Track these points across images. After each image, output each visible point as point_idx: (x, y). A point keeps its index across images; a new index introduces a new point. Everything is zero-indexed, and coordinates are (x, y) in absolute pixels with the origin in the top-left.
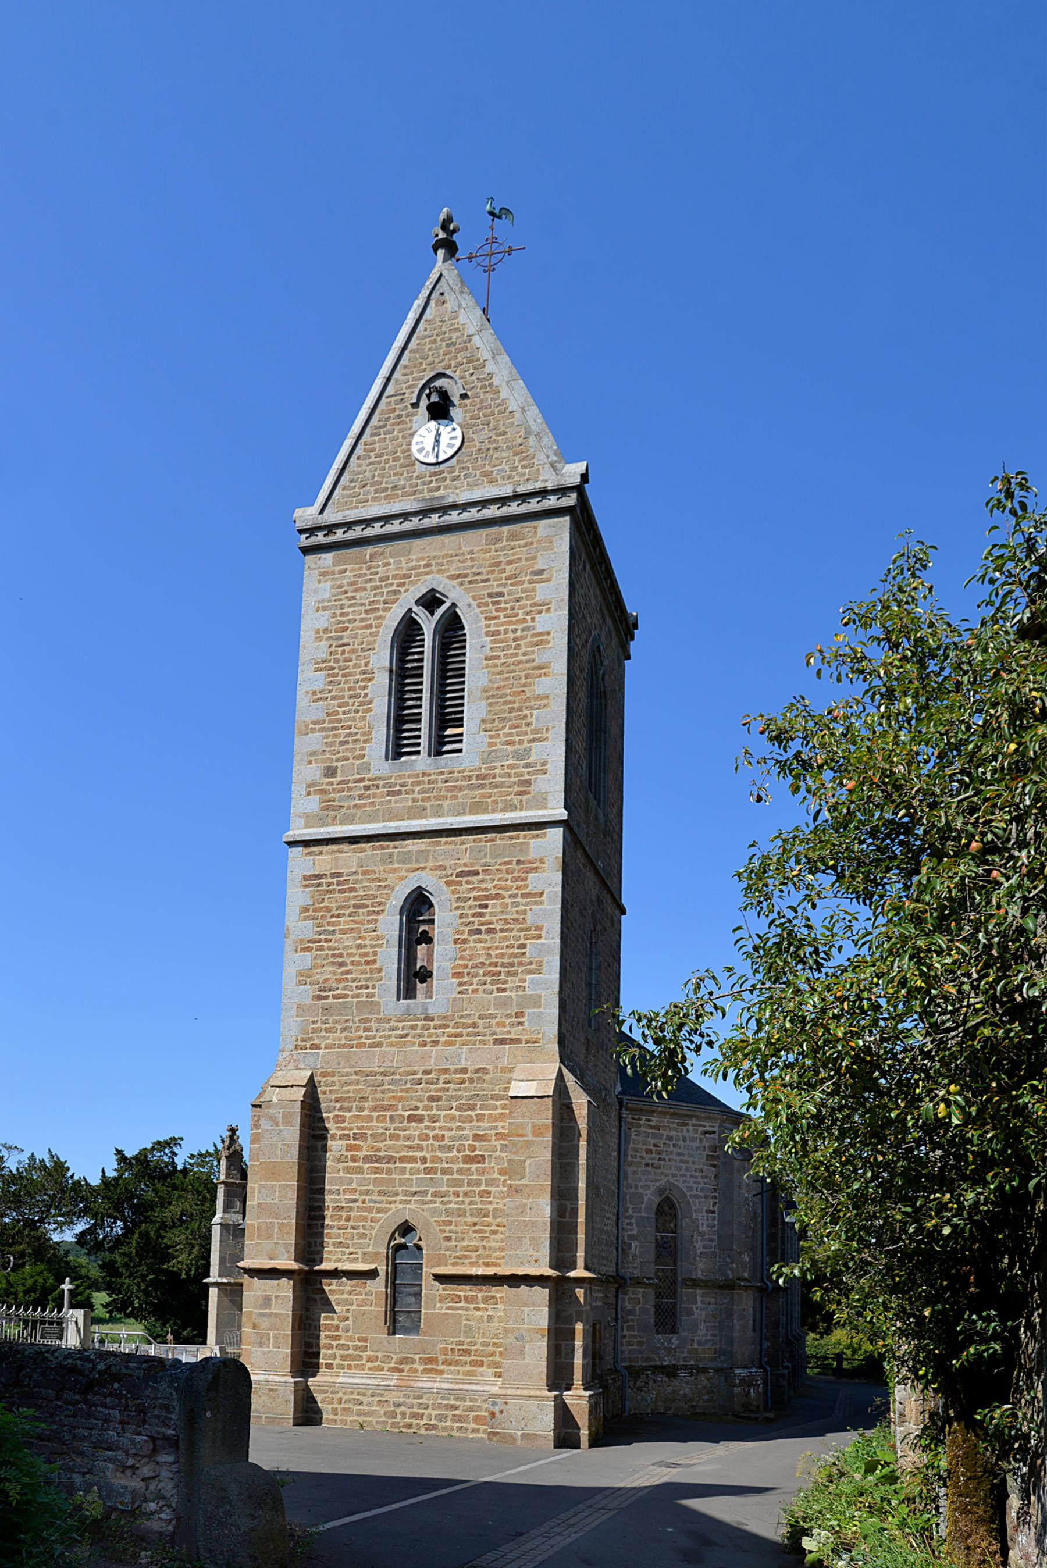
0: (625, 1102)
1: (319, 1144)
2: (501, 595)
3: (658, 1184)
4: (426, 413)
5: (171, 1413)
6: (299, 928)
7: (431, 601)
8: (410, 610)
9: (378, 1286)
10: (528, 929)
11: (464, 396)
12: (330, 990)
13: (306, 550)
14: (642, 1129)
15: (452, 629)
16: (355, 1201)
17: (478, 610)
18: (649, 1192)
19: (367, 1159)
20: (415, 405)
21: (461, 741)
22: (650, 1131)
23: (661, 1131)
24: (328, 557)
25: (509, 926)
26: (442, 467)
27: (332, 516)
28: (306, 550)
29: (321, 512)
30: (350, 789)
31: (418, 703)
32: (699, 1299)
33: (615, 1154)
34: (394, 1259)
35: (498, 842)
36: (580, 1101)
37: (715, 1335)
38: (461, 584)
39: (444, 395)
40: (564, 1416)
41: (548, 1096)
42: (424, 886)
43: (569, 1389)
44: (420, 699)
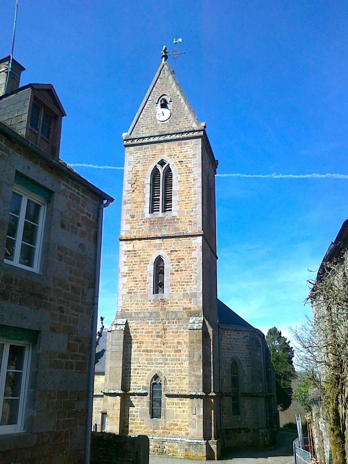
0: (220, 326)
1: (129, 345)
2: (182, 162)
3: (231, 356)
4: (160, 106)
5: (131, 454)
6: (124, 269)
7: (162, 163)
8: (156, 166)
9: (147, 399)
10: (193, 270)
11: (171, 101)
12: (132, 290)
13: (126, 146)
14: (226, 336)
15: (168, 171)
16: (140, 366)
17: (176, 166)
18: (229, 359)
19: (143, 351)
20: (157, 103)
21: (171, 207)
22: (228, 336)
23: (232, 336)
24: (132, 148)
25: (187, 269)
26: (164, 122)
27: (133, 136)
28: (126, 146)
29: (130, 135)
30: (138, 222)
31: (159, 195)
32: (246, 401)
33: (218, 346)
34: (152, 389)
35: (183, 241)
36: (210, 330)
37: (252, 416)
38: (171, 158)
39: (165, 101)
40: (209, 449)
41: (201, 329)
42: (161, 255)
43: (211, 440)
44: (159, 193)
